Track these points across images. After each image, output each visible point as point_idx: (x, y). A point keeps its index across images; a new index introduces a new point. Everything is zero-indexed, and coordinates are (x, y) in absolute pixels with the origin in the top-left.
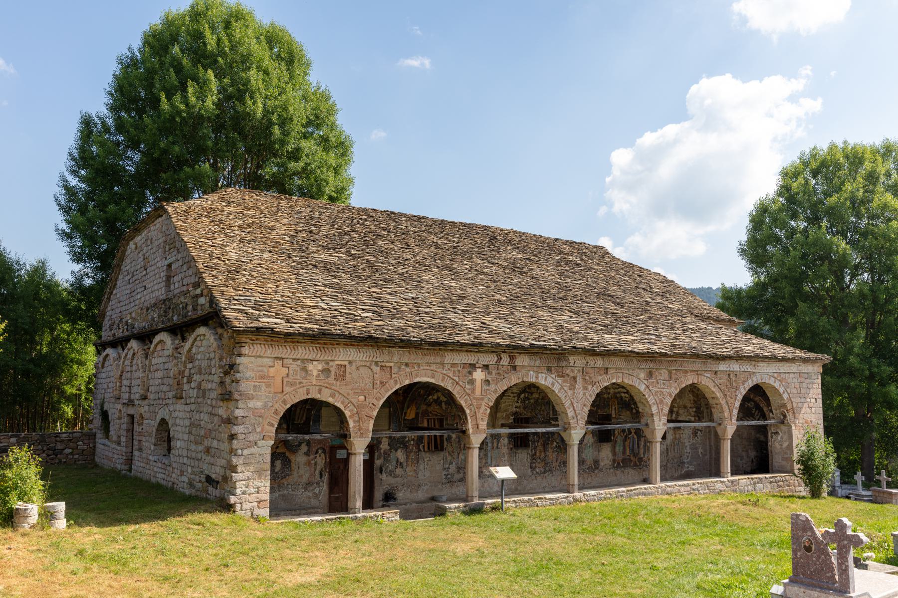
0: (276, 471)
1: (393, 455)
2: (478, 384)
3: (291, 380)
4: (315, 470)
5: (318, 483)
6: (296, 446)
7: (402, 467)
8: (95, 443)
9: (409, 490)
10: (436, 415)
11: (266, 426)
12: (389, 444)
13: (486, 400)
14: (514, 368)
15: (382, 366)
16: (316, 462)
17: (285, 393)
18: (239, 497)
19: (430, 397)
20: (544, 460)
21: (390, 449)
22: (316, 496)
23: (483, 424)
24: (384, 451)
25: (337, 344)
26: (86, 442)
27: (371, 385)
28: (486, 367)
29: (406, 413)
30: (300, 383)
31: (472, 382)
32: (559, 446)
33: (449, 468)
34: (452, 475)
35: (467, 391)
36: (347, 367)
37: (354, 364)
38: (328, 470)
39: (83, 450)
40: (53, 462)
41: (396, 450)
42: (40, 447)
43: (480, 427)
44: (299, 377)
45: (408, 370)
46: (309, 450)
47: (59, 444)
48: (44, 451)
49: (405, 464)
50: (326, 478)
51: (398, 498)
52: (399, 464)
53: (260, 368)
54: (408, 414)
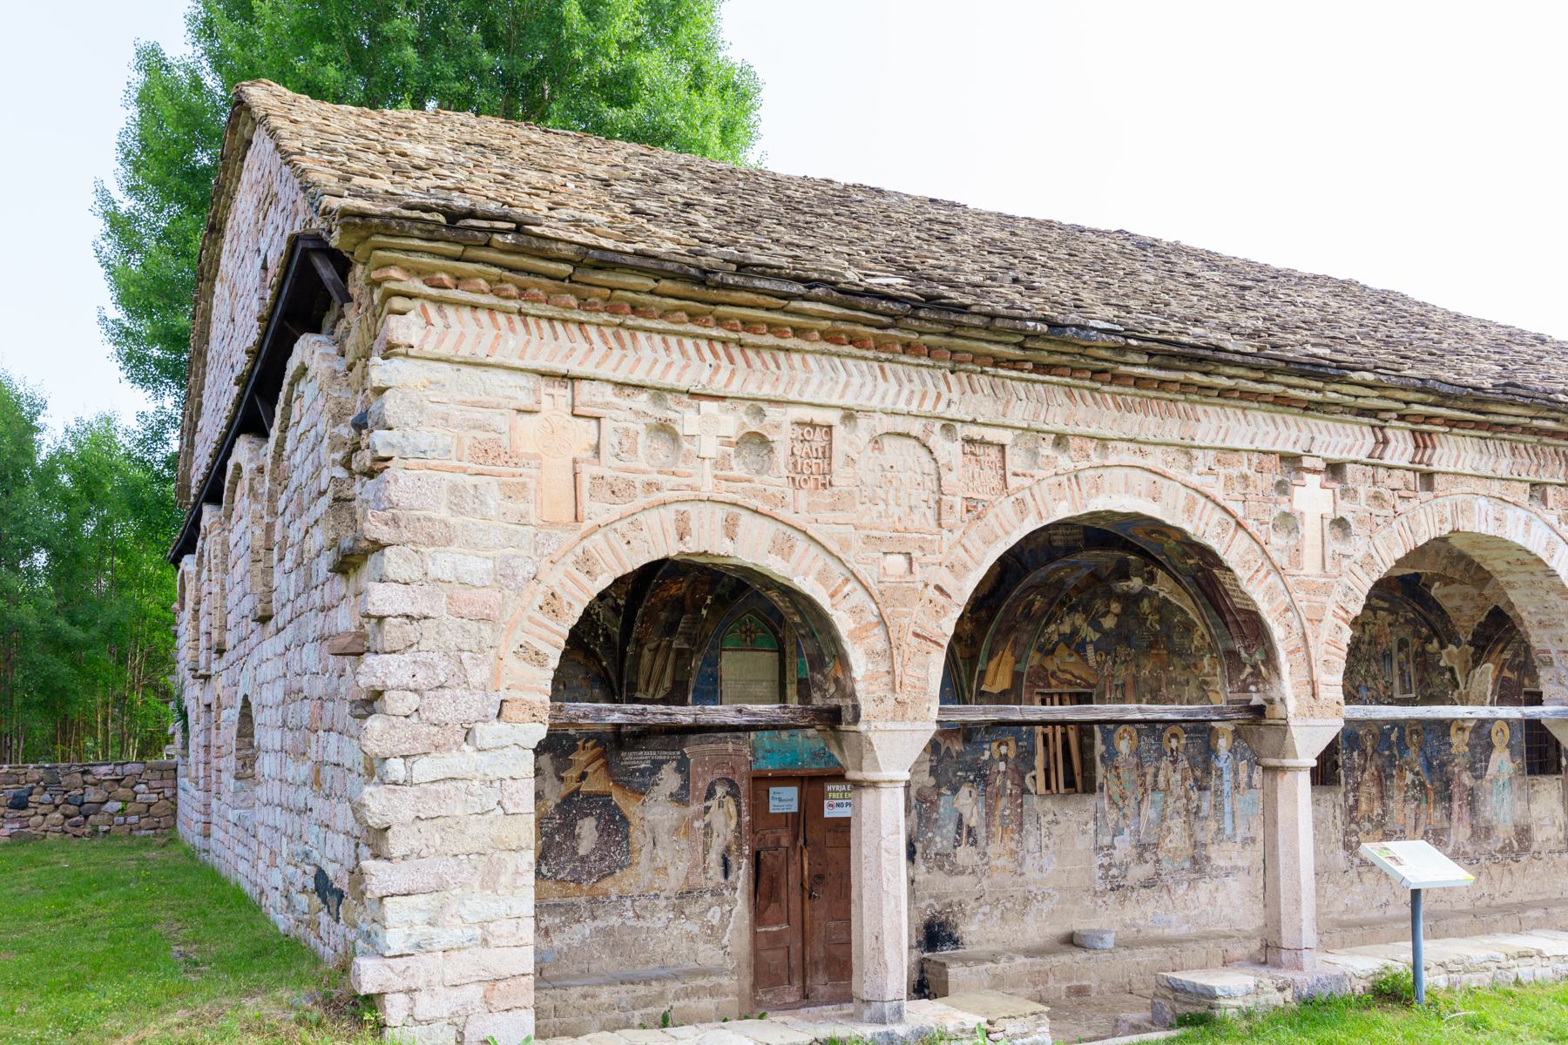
0: (582, 852)
1: (945, 805)
2: (1311, 530)
3: (608, 474)
4: (706, 850)
5: (717, 893)
6: (642, 772)
7: (975, 843)
8: (176, 787)
9: (997, 913)
10: (1070, 683)
11: (511, 662)
12: (933, 772)
13: (1337, 595)
14: (1428, 479)
15: (970, 441)
16: (708, 826)
17: (586, 525)
18: (400, 964)
19: (1052, 627)
20: (1380, 825)
21: (938, 786)
22: (713, 933)
23: (1332, 682)
24: (919, 792)
25: (798, 332)
26: (153, 784)
27: (931, 515)
28: (1335, 469)
29: (983, 673)
30: (650, 486)
31: (1288, 522)
32: (1422, 784)
33: (1112, 846)
34: (1124, 867)
35: (1274, 555)
36: (839, 432)
37: (862, 422)
38: (746, 850)
39: (150, 805)
40: (78, 832)
41: (955, 790)
42: (46, 797)
43: (1323, 693)
44: (643, 465)
45: (1064, 462)
46: (685, 787)
47: (91, 789)
48: (57, 807)
49: (981, 833)
50: (742, 873)
51: (966, 939)
52: (964, 832)
53: (479, 415)
54: (989, 677)
